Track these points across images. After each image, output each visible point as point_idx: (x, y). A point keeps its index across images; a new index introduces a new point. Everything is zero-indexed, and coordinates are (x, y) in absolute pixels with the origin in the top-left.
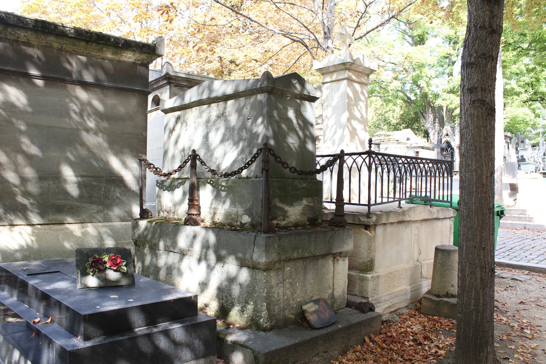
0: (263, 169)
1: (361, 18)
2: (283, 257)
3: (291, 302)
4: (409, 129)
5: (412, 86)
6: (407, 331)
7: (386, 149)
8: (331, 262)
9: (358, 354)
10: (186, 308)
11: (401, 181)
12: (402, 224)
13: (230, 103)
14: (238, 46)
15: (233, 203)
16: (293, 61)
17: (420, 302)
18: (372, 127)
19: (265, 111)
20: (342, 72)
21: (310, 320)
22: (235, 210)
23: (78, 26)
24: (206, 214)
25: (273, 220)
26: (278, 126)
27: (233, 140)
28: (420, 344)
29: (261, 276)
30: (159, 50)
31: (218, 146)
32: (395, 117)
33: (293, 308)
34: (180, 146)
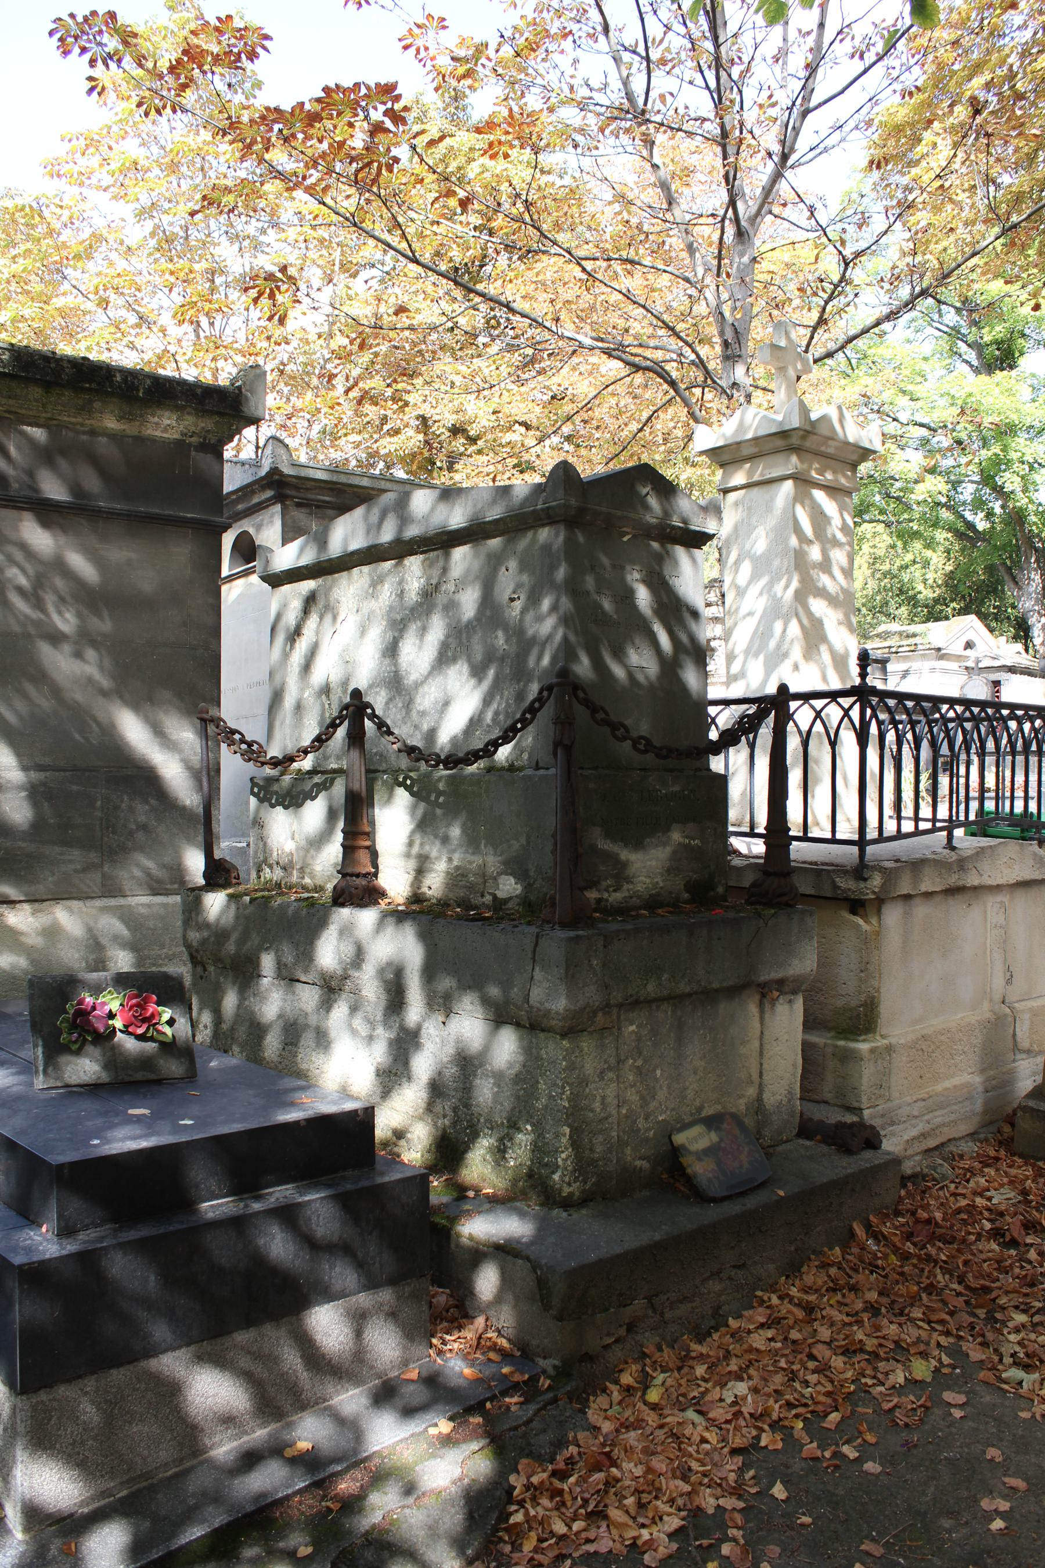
0: (557, 744)
1: (831, 298)
2: (617, 996)
3: (641, 1123)
4: (973, 617)
5: (977, 490)
6: (974, 1206)
7: (905, 674)
8: (753, 1009)
9: (833, 1271)
10: (345, 1141)
11: (950, 768)
12: (959, 897)
13: (460, 554)
14: (474, 388)
15: (472, 841)
16: (634, 426)
17: (1011, 1120)
18: (864, 610)
19: (561, 573)
20: (780, 458)
22: (478, 860)
23: (20, 339)
24: (395, 880)
25: (585, 888)
26: (601, 625)
27: (469, 661)
28: (1014, 1243)
29: (554, 1049)
30: (252, 403)
31: (426, 678)
32: (930, 582)
33: (647, 1140)
34: (319, 675)
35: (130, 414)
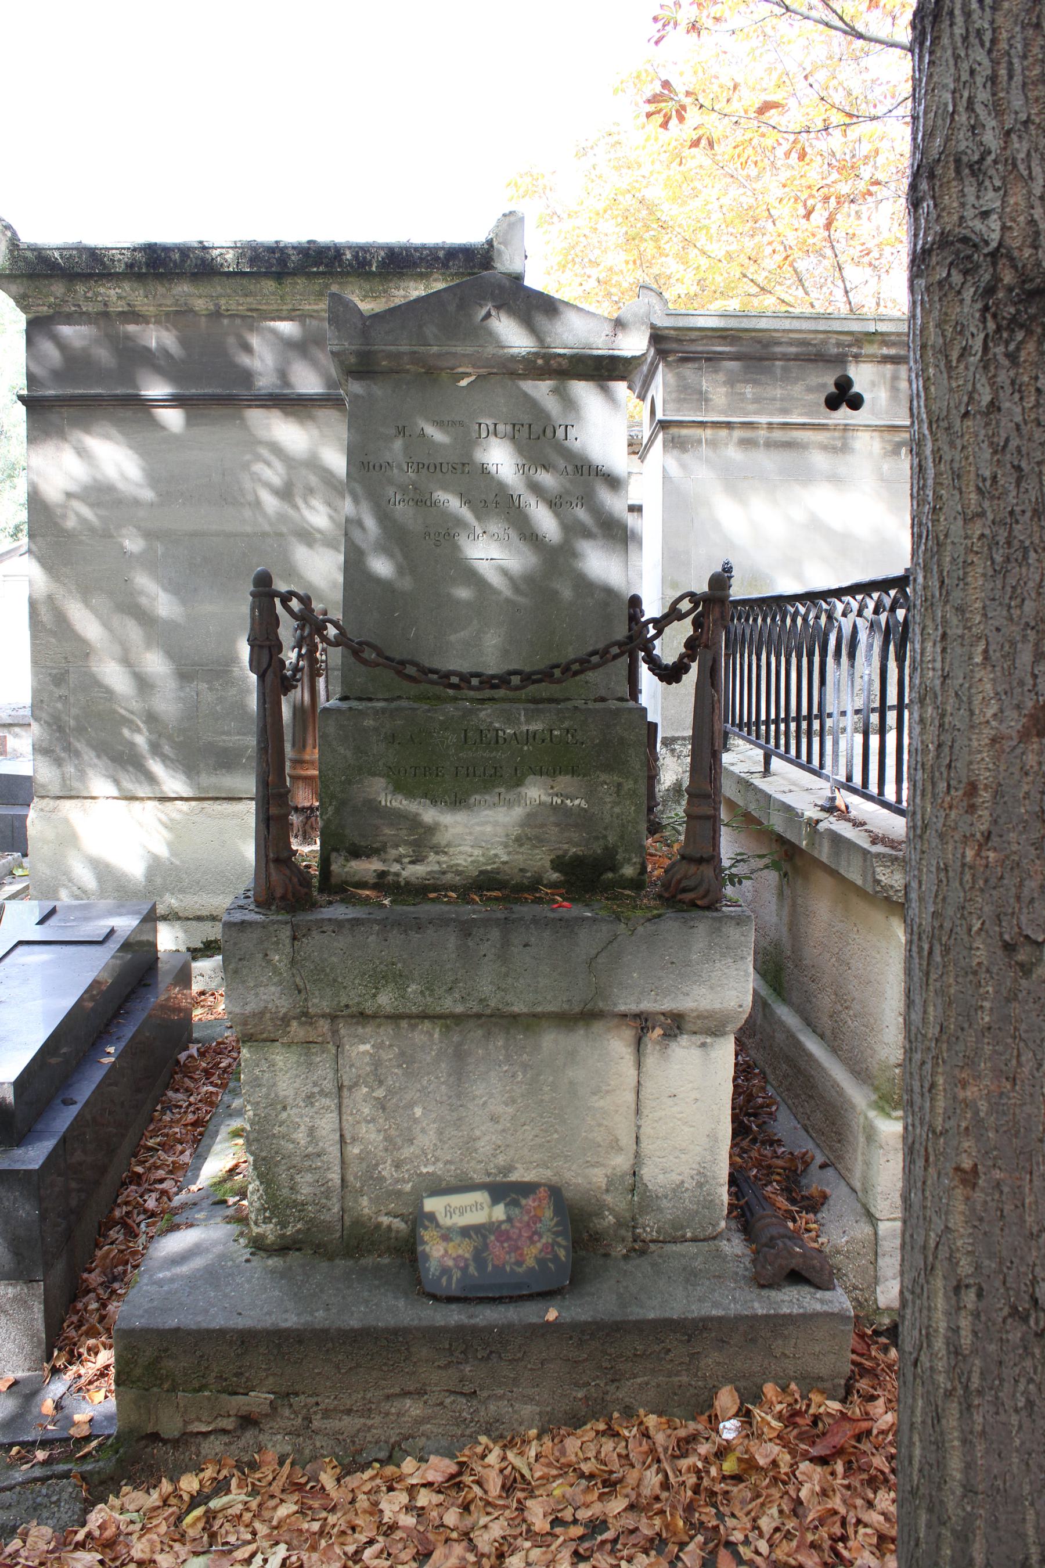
2: (319, 1003)
3: (387, 1171)
21: (427, 1257)
30: (506, 257)
35: (372, 291)
